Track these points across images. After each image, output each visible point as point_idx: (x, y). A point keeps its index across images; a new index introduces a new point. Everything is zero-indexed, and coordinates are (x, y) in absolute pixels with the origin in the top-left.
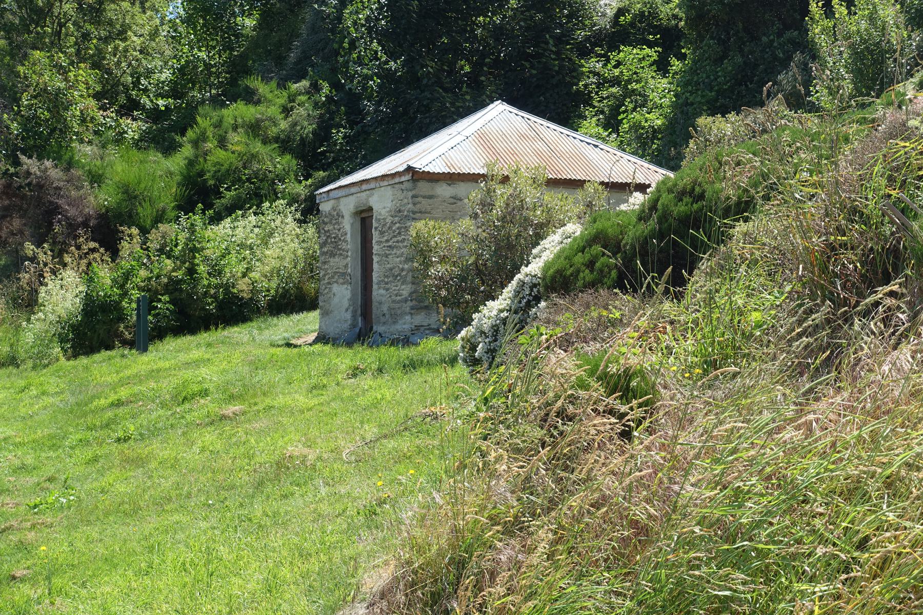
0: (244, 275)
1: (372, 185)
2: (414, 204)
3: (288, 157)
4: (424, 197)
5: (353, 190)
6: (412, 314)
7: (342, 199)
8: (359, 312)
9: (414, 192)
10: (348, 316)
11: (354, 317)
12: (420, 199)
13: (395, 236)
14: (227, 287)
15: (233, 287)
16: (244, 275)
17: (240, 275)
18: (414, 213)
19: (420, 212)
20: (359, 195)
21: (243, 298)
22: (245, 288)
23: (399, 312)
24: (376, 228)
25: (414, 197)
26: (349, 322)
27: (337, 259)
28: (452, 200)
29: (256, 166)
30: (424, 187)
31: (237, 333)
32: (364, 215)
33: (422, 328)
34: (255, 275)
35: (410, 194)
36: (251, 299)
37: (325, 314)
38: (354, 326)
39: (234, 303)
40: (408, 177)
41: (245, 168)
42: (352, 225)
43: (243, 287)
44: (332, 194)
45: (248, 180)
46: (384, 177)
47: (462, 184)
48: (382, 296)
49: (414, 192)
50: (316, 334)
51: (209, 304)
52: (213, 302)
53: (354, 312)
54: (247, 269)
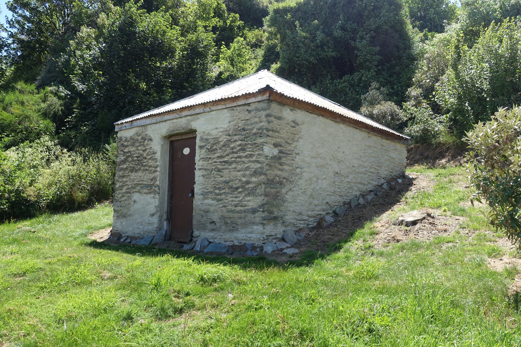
0: (31, 185)
1: (197, 111)
2: (269, 122)
3: (48, 121)
4: (275, 117)
5: (167, 117)
6: (263, 224)
7: (148, 126)
8: (165, 217)
9: (268, 112)
10: (155, 220)
11: (160, 221)
12: (272, 119)
13: (233, 153)
14: (18, 192)
15: (23, 193)
16: (31, 185)
17: (28, 184)
18: (268, 130)
19: (273, 131)
20: (175, 121)
21: (30, 201)
22: (32, 193)
23: (239, 221)
24: (201, 147)
25: (268, 116)
26: (156, 226)
27: (140, 173)
28: (294, 125)
29: (27, 124)
30: (275, 108)
31: (25, 225)
32: (173, 139)
33: (270, 238)
34: (39, 185)
35: (264, 113)
36: (36, 201)
37: (119, 215)
38: (160, 228)
39: (23, 204)
40: (266, 96)
41: (19, 124)
42: (162, 146)
43: (30, 193)
44: (135, 123)
45: (22, 131)
46: (204, 104)
47: (299, 111)
48: (210, 205)
49: (268, 112)
50: (109, 230)
51: (3, 205)
52: (7, 203)
53: (161, 217)
54: (32, 181)
